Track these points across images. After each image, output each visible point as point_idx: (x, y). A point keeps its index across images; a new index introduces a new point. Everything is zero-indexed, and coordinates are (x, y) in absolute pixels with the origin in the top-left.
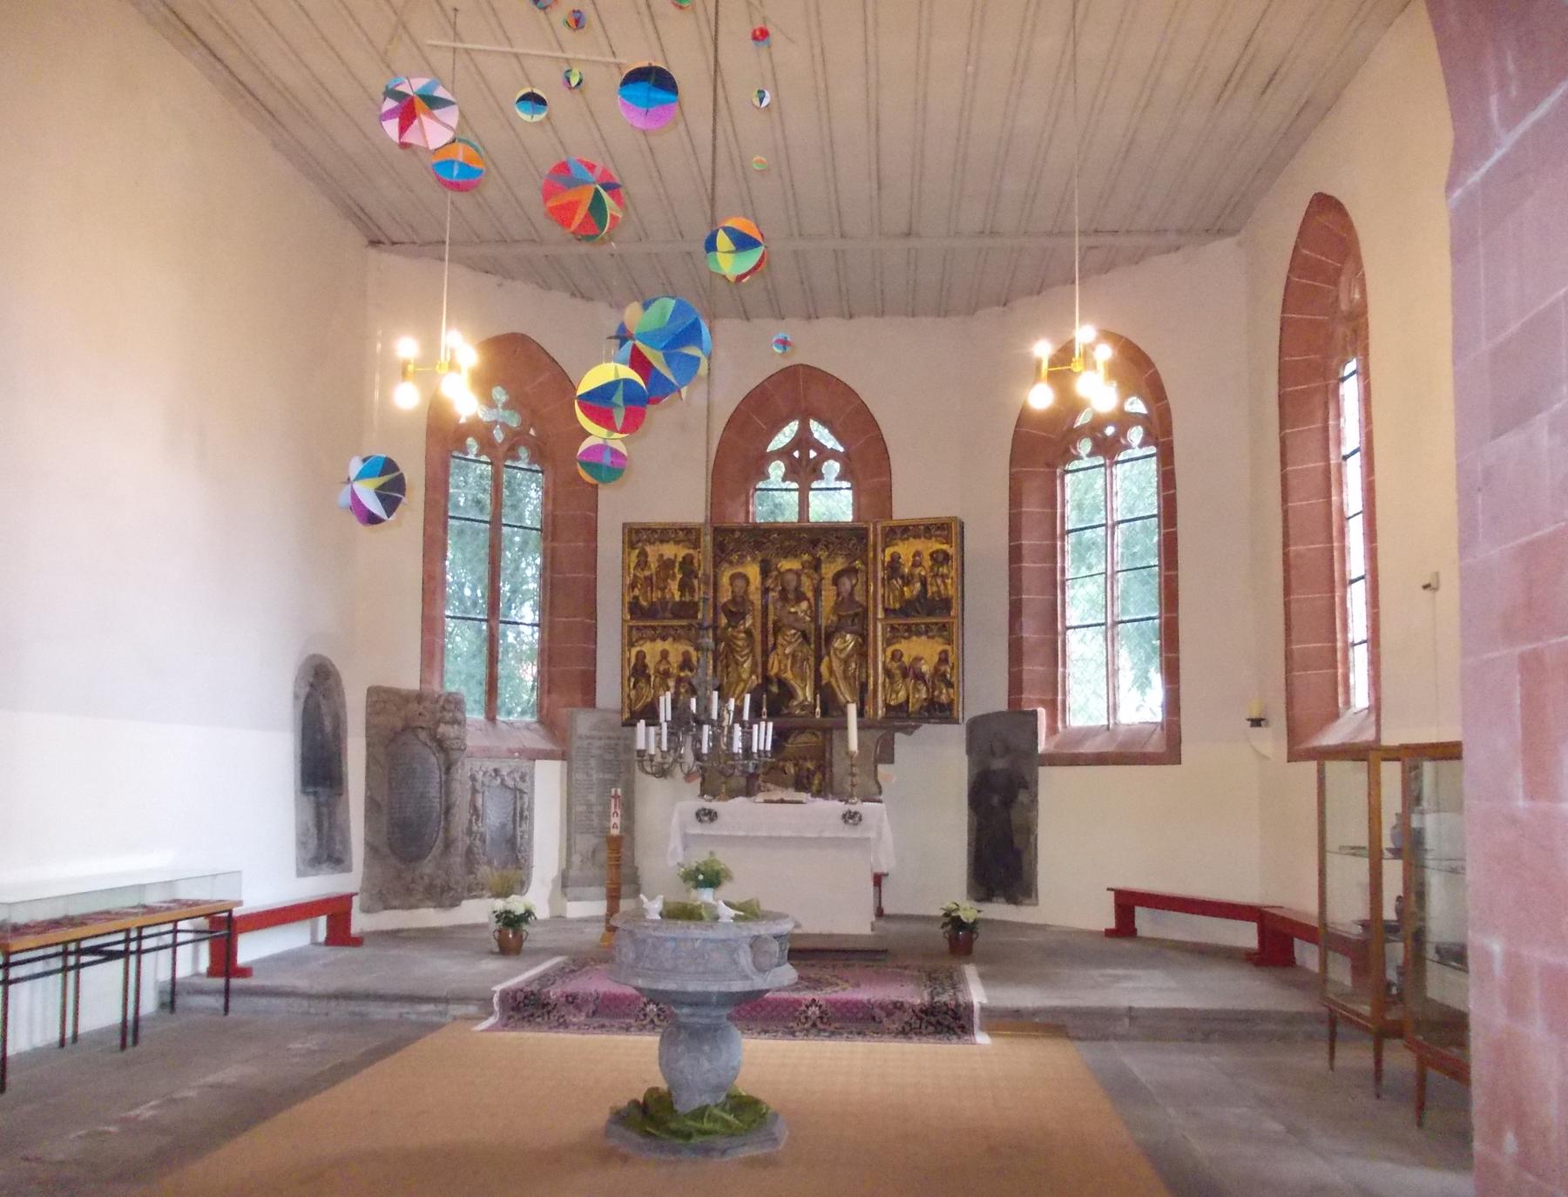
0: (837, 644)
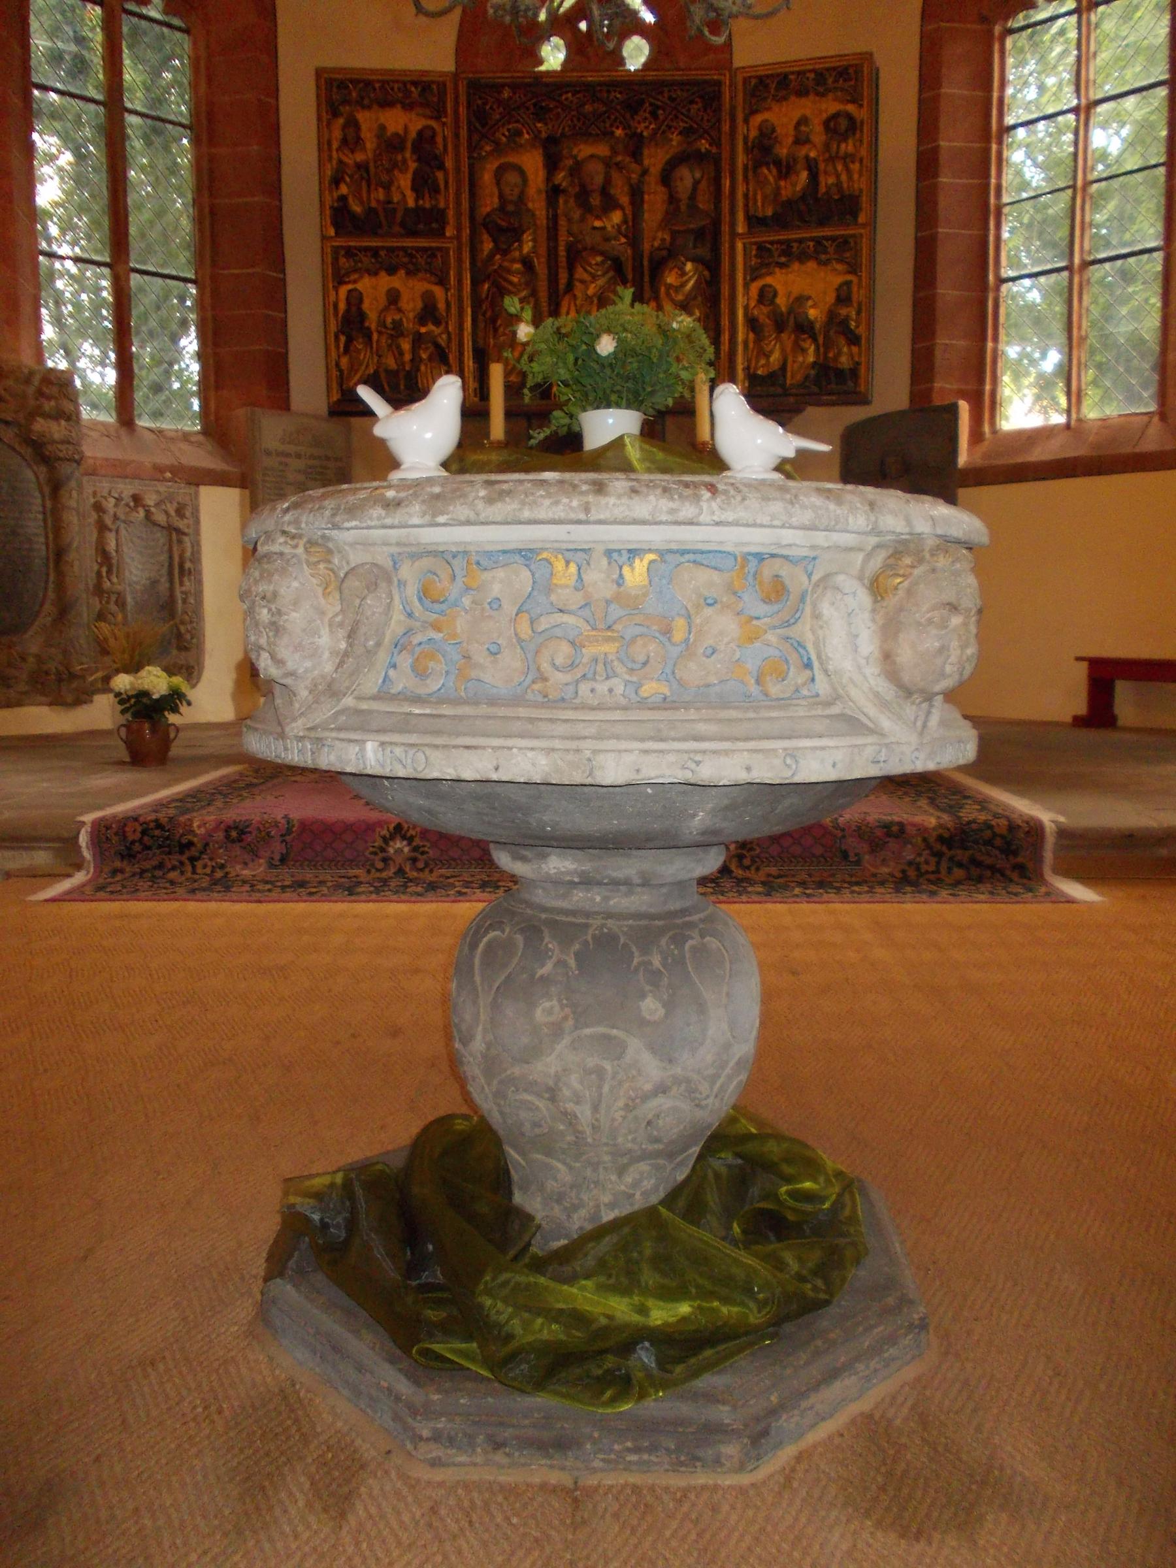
0: (671, 279)
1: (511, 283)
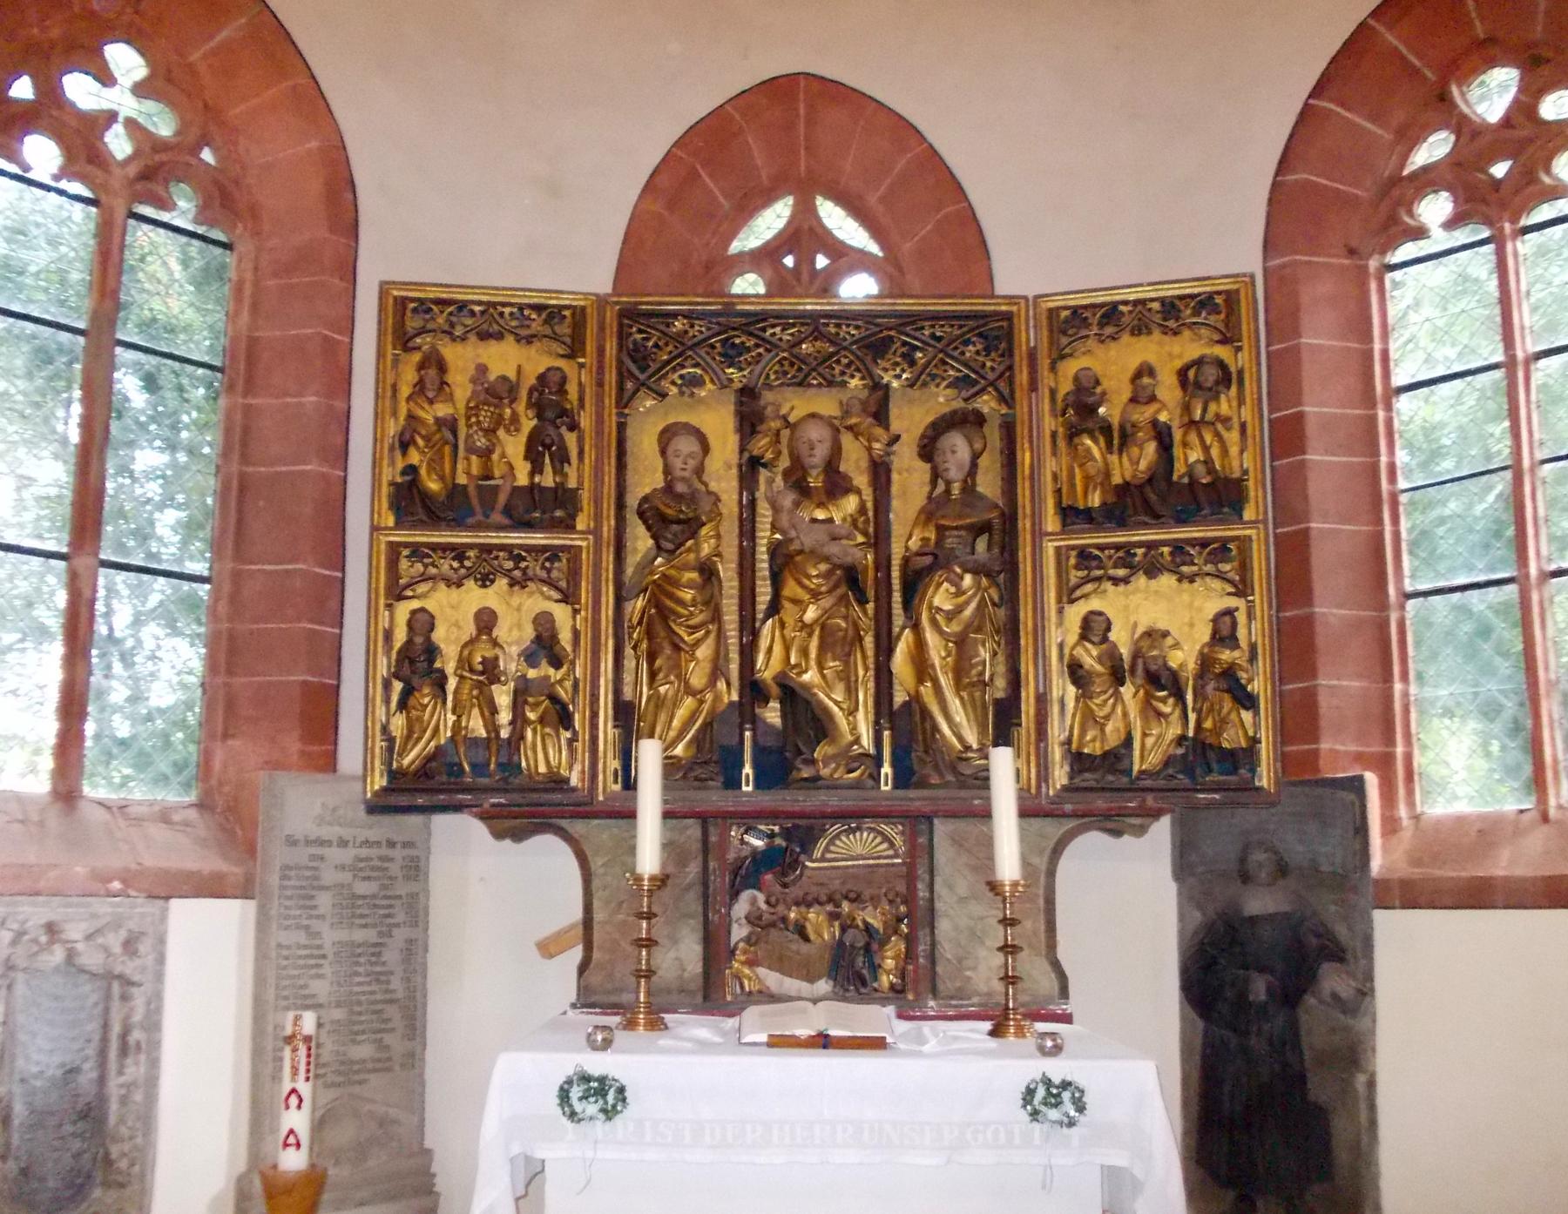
1: (681, 602)
